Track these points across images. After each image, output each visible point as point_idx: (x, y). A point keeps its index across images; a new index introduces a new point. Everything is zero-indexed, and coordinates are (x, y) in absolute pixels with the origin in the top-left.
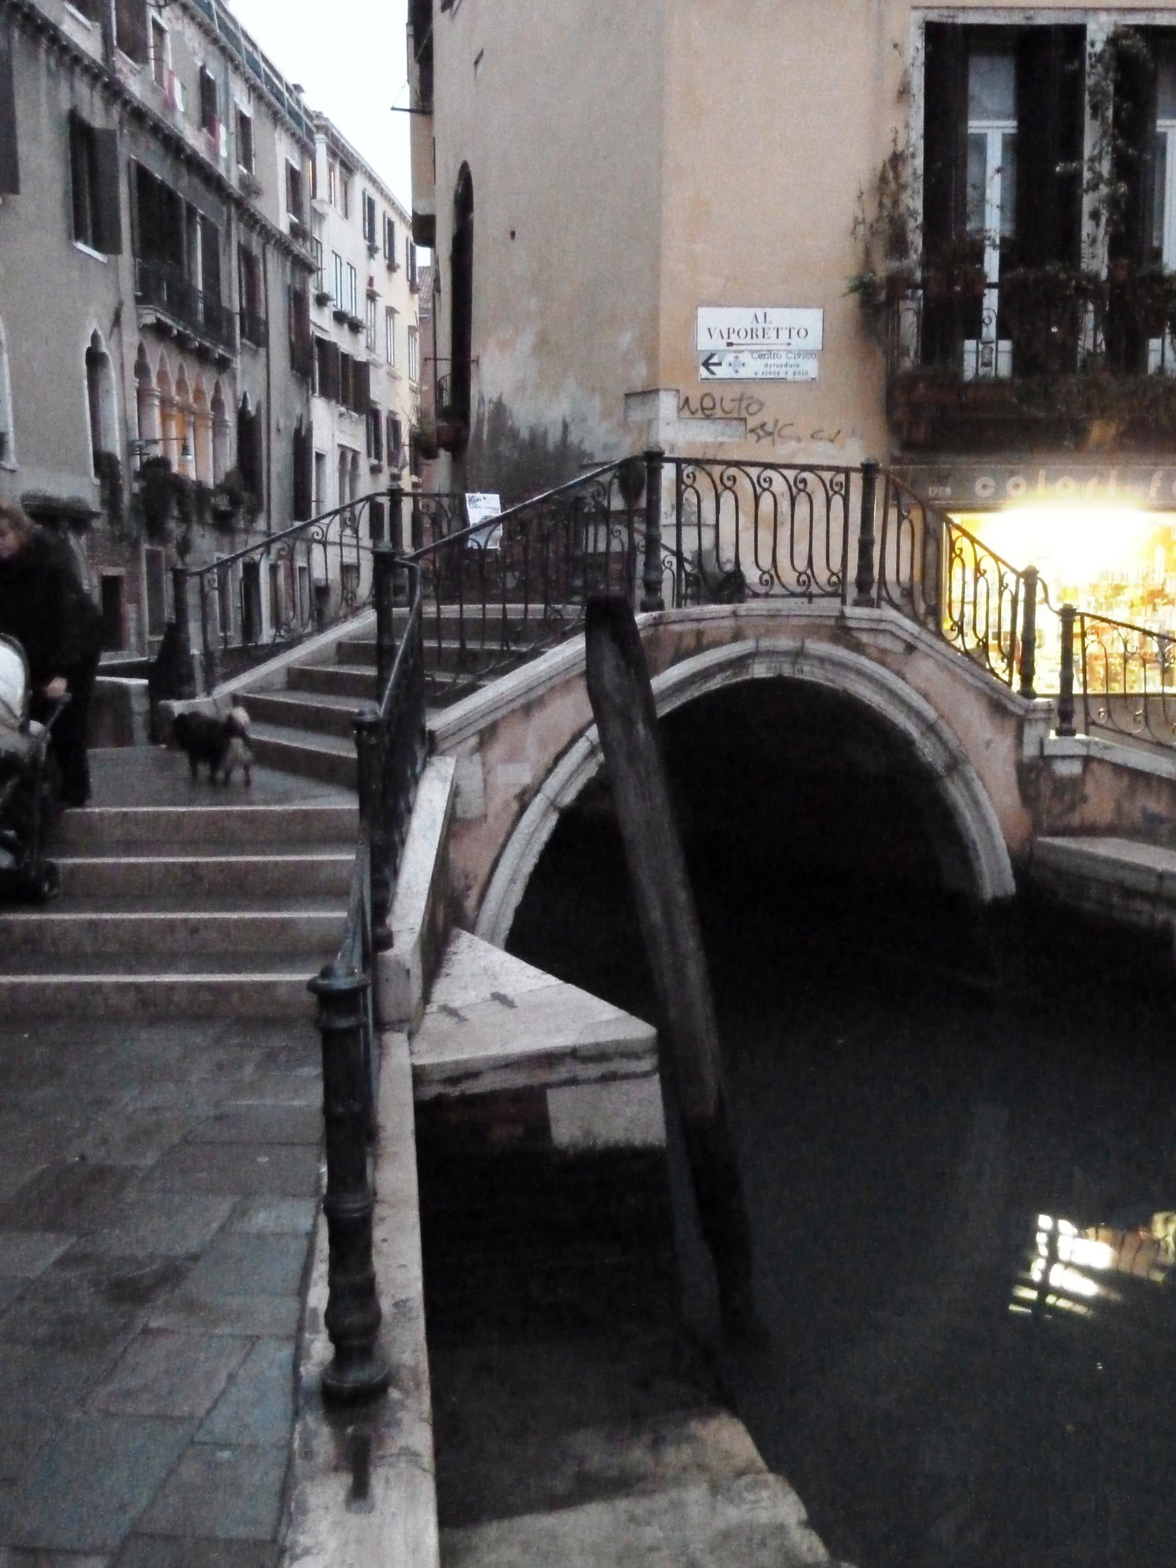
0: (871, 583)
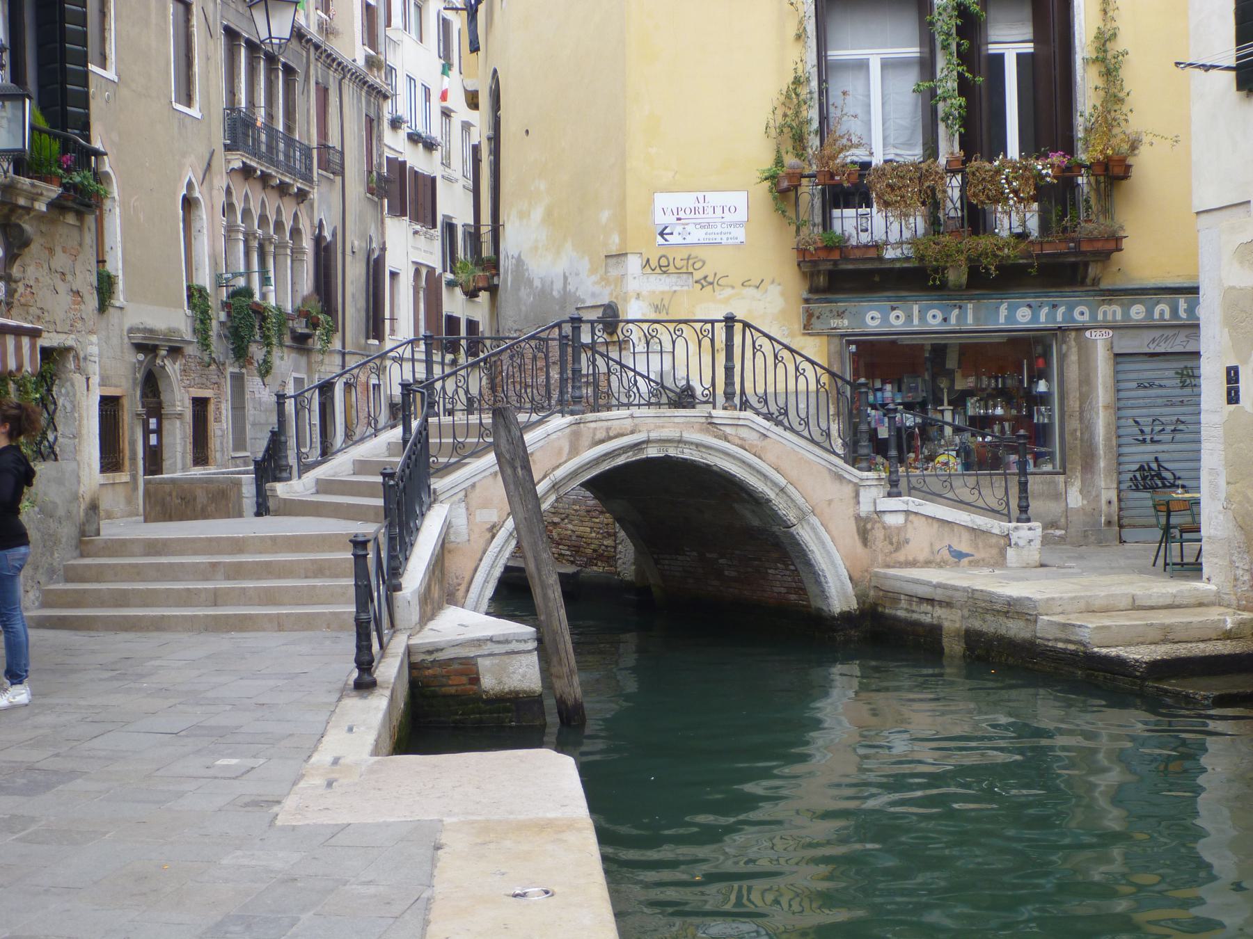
0: (734, 394)
